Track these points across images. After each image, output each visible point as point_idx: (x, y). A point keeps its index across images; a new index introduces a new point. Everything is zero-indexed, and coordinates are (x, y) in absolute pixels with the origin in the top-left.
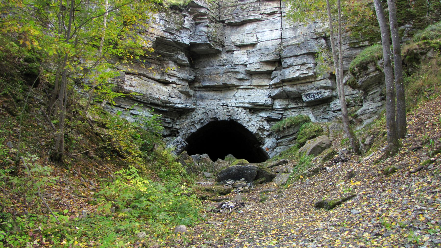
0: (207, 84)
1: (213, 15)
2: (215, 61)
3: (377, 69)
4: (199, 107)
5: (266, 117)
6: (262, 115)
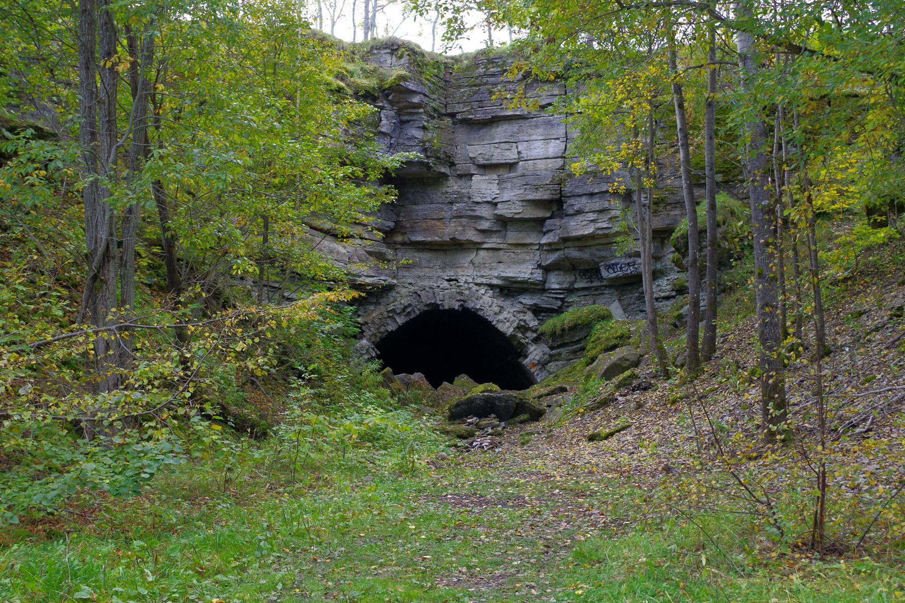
0: (420, 238)
1: (433, 105)
2: (437, 195)
4: (401, 281)
5: (531, 305)
6: (524, 301)
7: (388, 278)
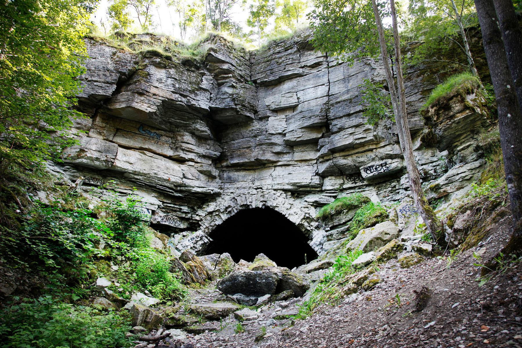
0: (236, 161)
1: (240, 73)
2: (246, 132)
3: (466, 107)
4: (226, 191)
5: (313, 202)
6: (308, 200)
7: (215, 189)
